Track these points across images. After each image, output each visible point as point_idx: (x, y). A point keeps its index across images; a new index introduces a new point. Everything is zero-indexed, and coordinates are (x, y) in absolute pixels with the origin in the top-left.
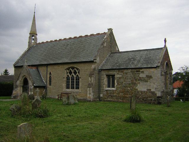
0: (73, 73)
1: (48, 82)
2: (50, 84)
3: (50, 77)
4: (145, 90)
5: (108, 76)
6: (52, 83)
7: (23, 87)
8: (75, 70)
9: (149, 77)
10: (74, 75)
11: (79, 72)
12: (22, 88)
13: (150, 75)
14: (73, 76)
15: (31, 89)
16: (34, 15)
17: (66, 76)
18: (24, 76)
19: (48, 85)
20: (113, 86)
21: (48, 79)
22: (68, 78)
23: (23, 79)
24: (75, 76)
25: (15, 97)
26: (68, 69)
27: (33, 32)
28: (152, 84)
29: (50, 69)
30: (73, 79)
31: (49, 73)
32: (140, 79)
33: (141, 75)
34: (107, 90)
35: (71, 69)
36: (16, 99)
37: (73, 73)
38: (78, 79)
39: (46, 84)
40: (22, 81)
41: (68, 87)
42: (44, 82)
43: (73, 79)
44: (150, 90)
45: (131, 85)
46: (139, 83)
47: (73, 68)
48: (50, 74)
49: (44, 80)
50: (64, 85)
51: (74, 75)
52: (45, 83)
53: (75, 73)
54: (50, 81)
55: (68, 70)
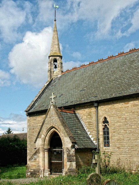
1: (101, 139)
2: (107, 143)
3: (104, 129)
6: (110, 140)
7: (50, 152)
12: (46, 154)
15: (67, 142)
18: (52, 127)
19: (102, 145)
21: (101, 133)
23: (49, 134)
25: (34, 174)
27: (55, 53)
29: (103, 109)
31: (101, 119)
36: (35, 177)
39: (96, 144)
40: (47, 138)
42: (92, 139)
48: (105, 121)
49: (90, 136)
52: (94, 142)
54: (106, 132)
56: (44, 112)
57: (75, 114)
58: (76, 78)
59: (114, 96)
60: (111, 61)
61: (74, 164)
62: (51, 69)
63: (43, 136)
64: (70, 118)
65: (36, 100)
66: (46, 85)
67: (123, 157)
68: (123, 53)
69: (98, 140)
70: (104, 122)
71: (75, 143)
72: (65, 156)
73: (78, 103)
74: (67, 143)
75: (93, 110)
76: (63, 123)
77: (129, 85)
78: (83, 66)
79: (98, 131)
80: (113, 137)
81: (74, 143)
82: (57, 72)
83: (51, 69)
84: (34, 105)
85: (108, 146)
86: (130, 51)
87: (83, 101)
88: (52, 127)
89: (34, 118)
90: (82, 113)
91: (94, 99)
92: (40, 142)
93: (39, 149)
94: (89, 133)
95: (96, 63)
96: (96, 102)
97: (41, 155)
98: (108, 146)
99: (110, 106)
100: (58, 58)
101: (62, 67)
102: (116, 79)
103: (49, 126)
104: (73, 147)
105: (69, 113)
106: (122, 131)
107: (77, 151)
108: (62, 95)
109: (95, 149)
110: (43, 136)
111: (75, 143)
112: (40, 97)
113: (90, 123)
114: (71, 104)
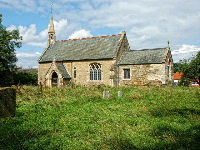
0: (95, 68)
1: (73, 75)
4: (154, 80)
5: (125, 70)
8: (97, 65)
9: (157, 70)
10: (96, 69)
11: (101, 67)
12: (51, 81)
13: (157, 68)
14: (95, 70)
16: (168, 44)
17: (89, 70)
18: (54, 70)
19: (73, 77)
20: (129, 77)
21: (73, 73)
22: (91, 72)
23: (52, 73)
24: (97, 70)
26: (91, 64)
28: (159, 75)
29: (74, 63)
30: (95, 72)
31: (73, 68)
32: (150, 72)
33: (151, 69)
34: (124, 81)
35: (93, 64)
37: (95, 68)
38: (100, 72)
40: (51, 74)
41: (91, 79)
42: (70, 75)
43: (95, 72)
44: (157, 79)
45: (143, 76)
46: (149, 75)
47: (95, 64)
48: (75, 68)
49: (69, 74)
50: (88, 77)
51: (96, 69)
52: (70, 76)
53: (97, 67)
54: (75, 72)
55: (91, 65)
56: (51, 62)
57: (63, 64)
58: (63, 47)
59: (78, 59)
60: (79, 41)
61: (63, 84)
62: (49, 39)
63: (49, 73)
64: (61, 66)
65: (43, 56)
66: (47, 48)
67: (81, 82)
68: (99, 37)
69: (72, 75)
70: (74, 69)
71: (63, 76)
72: (59, 81)
73: (64, 60)
74: (60, 76)
75: (70, 63)
76: (59, 69)
77: (85, 55)
78: (103, 36)
79: (72, 72)
80: (78, 74)
81: (63, 76)
82: (52, 41)
83: (49, 39)
84: (41, 58)
85: (101, 79)
86: (97, 37)
87: (66, 59)
88: (54, 70)
89: (43, 64)
90: (66, 64)
91: (71, 59)
92: (48, 76)
93: (47, 79)
94: (68, 72)
95: (73, 40)
96: (72, 61)
97: (48, 81)
98: (101, 79)
99: (77, 63)
100: (53, 34)
101: (55, 39)
102: (80, 51)
103: (52, 70)
104: (62, 78)
105: (60, 64)
106: (81, 72)
107: (64, 79)
108: (56, 55)
109: (71, 79)
110: (49, 73)
111: (63, 76)
112: (44, 54)
113: (69, 69)
114: (61, 60)
